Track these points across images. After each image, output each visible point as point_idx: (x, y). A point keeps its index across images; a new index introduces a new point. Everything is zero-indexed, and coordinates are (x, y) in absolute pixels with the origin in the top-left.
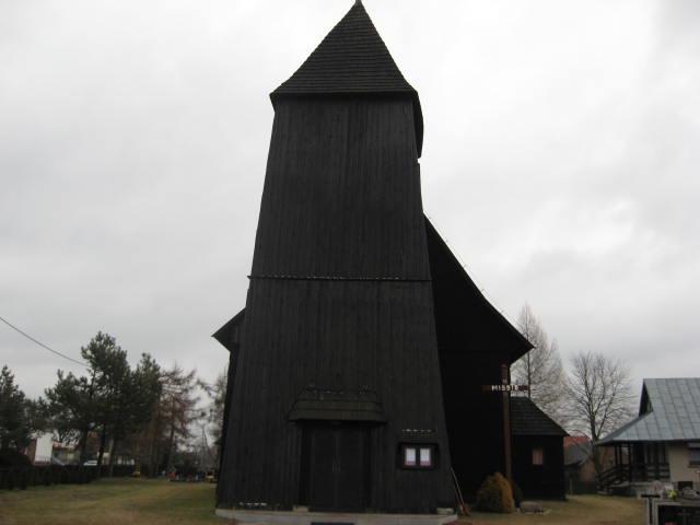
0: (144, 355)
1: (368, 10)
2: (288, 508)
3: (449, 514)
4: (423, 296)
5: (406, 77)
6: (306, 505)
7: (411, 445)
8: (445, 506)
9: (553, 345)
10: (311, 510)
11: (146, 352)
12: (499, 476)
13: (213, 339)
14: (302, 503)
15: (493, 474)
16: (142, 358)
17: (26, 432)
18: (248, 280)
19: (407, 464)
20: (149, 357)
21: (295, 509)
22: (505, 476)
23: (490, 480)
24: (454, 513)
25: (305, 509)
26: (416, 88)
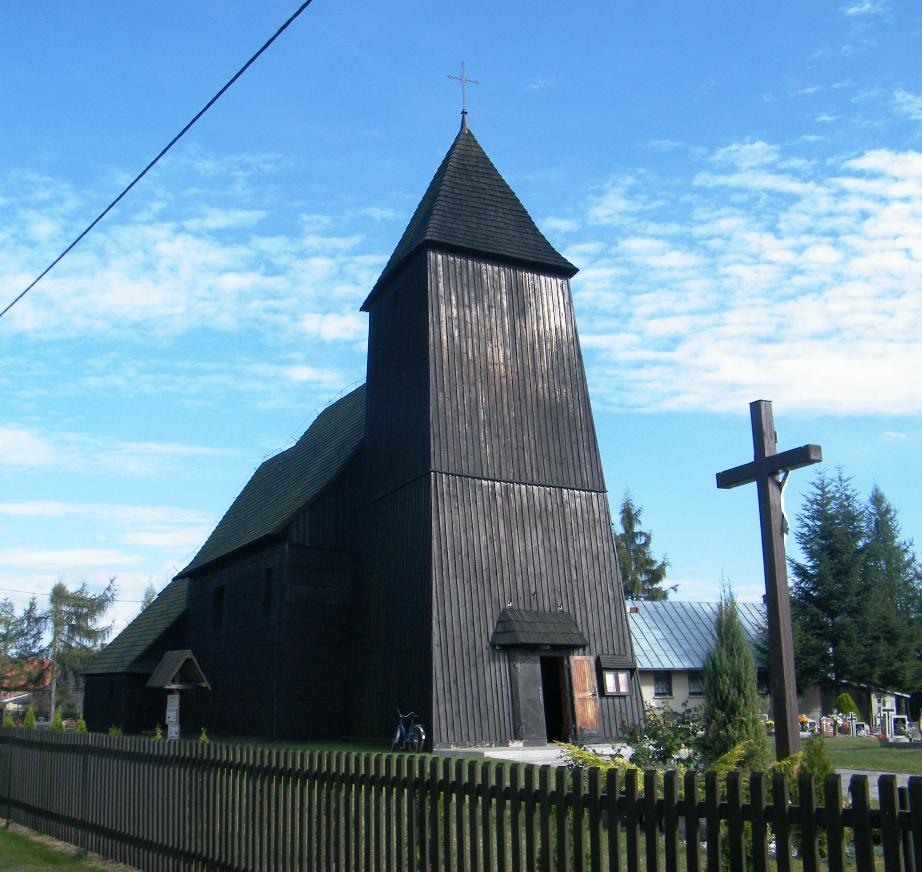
6: (521, 739)
10: (525, 745)
14: (517, 736)
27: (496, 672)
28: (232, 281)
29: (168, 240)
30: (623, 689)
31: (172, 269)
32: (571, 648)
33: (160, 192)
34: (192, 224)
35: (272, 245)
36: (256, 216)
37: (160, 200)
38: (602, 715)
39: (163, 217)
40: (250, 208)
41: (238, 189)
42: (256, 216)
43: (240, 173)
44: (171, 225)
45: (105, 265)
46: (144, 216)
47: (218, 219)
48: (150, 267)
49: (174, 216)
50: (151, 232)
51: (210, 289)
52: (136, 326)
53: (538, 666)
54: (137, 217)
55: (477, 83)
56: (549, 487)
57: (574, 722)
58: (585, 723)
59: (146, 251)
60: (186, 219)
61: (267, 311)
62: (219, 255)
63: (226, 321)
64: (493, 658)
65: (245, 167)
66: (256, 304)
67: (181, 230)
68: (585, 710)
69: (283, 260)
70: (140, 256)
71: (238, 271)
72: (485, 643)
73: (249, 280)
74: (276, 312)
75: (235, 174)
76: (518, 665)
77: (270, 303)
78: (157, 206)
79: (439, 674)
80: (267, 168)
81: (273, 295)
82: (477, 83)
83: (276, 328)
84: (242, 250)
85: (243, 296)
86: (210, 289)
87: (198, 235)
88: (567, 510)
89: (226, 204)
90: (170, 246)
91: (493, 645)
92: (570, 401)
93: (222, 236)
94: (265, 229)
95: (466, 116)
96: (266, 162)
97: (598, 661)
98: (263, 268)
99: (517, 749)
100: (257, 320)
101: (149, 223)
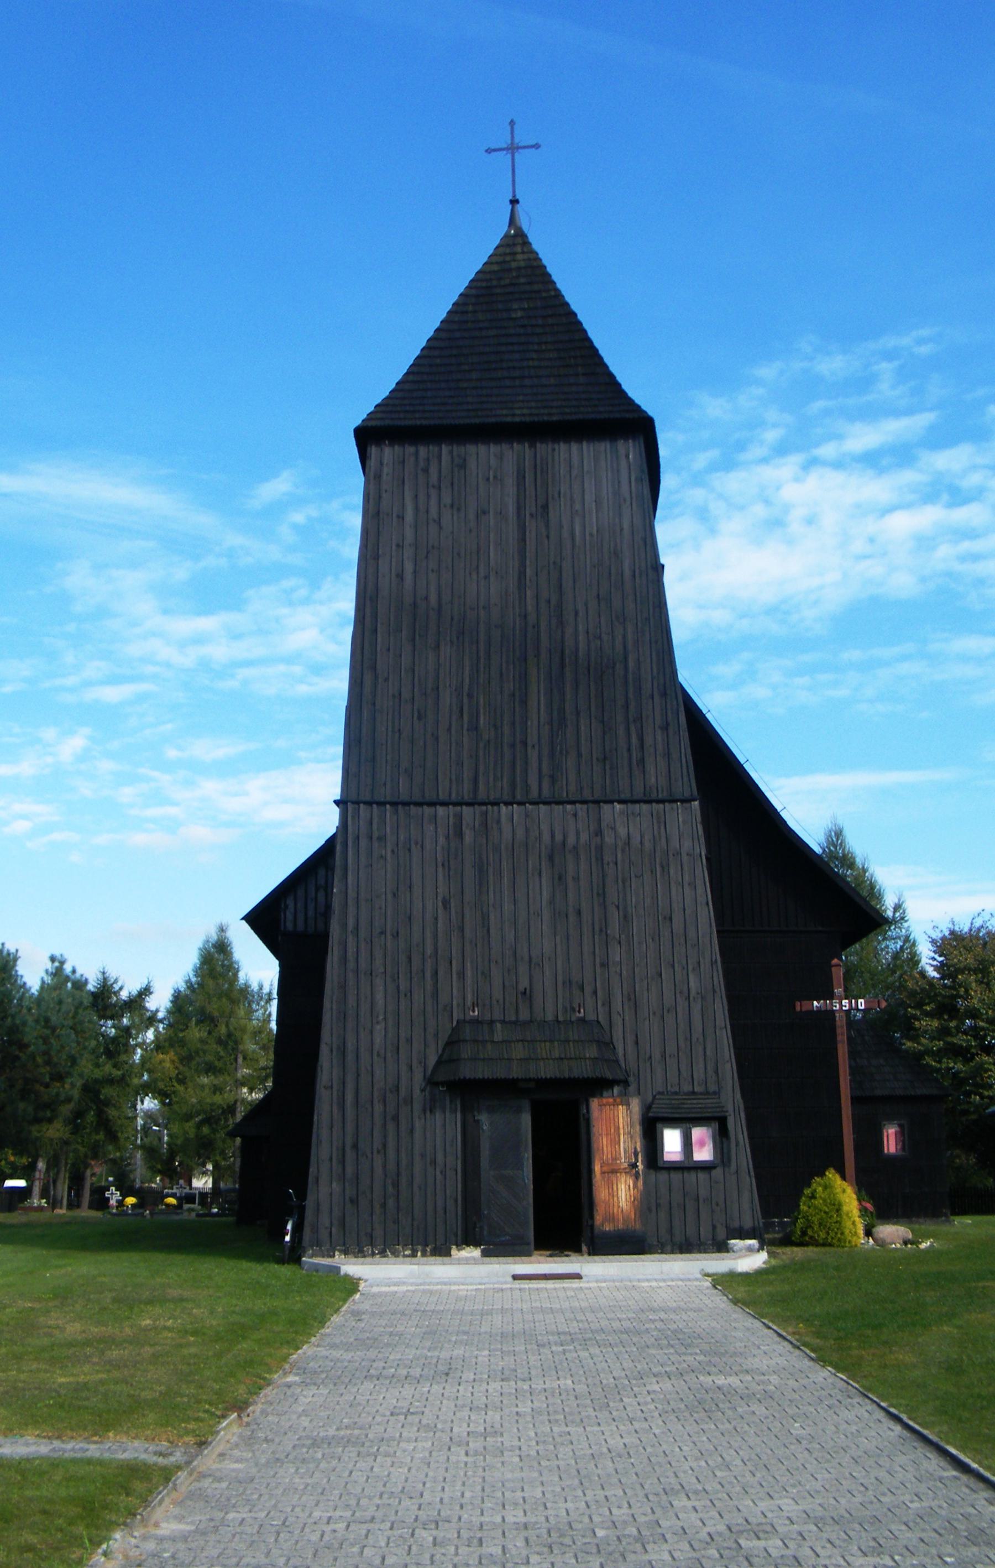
0: (53, 959)
1: (538, 243)
2: (441, 1251)
3: (750, 1249)
4: (685, 826)
5: (625, 387)
6: (476, 1244)
7: (673, 1122)
8: (742, 1234)
9: (897, 907)
10: (485, 1254)
11: (57, 954)
12: (831, 1175)
13: (244, 922)
14: (469, 1240)
15: (822, 1174)
16: (49, 965)
17: (209, 1158)
18: (336, 811)
19: (667, 1158)
20: (62, 963)
21: (454, 1251)
22: (844, 1178)
23: (817, 1184)
24: (761, 1248)
25: (476, 1253)
26: (651, 413)
27: (441, 1131)
28: (903, 524)
29: (797, 480)
30: (703, 1154)
31: (810, 521)
32: (599, 1086)
33: (772, 415)
34: (828, 451)
35: (951, 460)
36: (925, 419)
37: (775, 426)
38: (647, 1203)
39: (782, 450)
40: (910, 411)
41: (885, 389)
42: (925, 419)
43: (884, 365)
44: (794, 461)
45: (713, 531)
46: (756, 452)
47: (864, 438)
48: (776, 523)
49: (800, 443)
50: (768, 473)
51: (872, 540)
52: (772, 611)
53: (526, 1120)
54: (742, 457)
55: (537, 146)
56: (573, 803)
57: (592, 1217)
58: (611, 1218)
59: (767, 502)
60: (817, 445)
61: (962, 559)
62: (876, 489)
63: (903, 584)
64: (430, 1107)
65: (889, 356)
66: (944, 551)
67: (811, 464)
68: (613, 1194)
69: (975, 479)
70: (759, 510)
71: (907, 506)
72: (418, 1077)
73: (929, 517)
74: (976, 557)
75: (876, 368)
76: (484, 1118)
77: (966, 546)
78: (771, 436)
79: (324, 1133)
80: (925, 350)
81: (970, 534)
82: (537, 146)
83: (980, 582)
84: (909, 476)
85: (924, 543)
86: (872, 540)
87: (838, 464)
88: (609, 839)
89: (871, 414)
90: (802, 489)
91: (431, 1082)
92: (630, 647)
93: (872, 461)
94: (939, 438)
95: (518, 207)
96: (920, 342)
97: (647, 1108)
98: (945, 497)
99: (467, 1261)
100: (949, 574)
101: (764, 461)
